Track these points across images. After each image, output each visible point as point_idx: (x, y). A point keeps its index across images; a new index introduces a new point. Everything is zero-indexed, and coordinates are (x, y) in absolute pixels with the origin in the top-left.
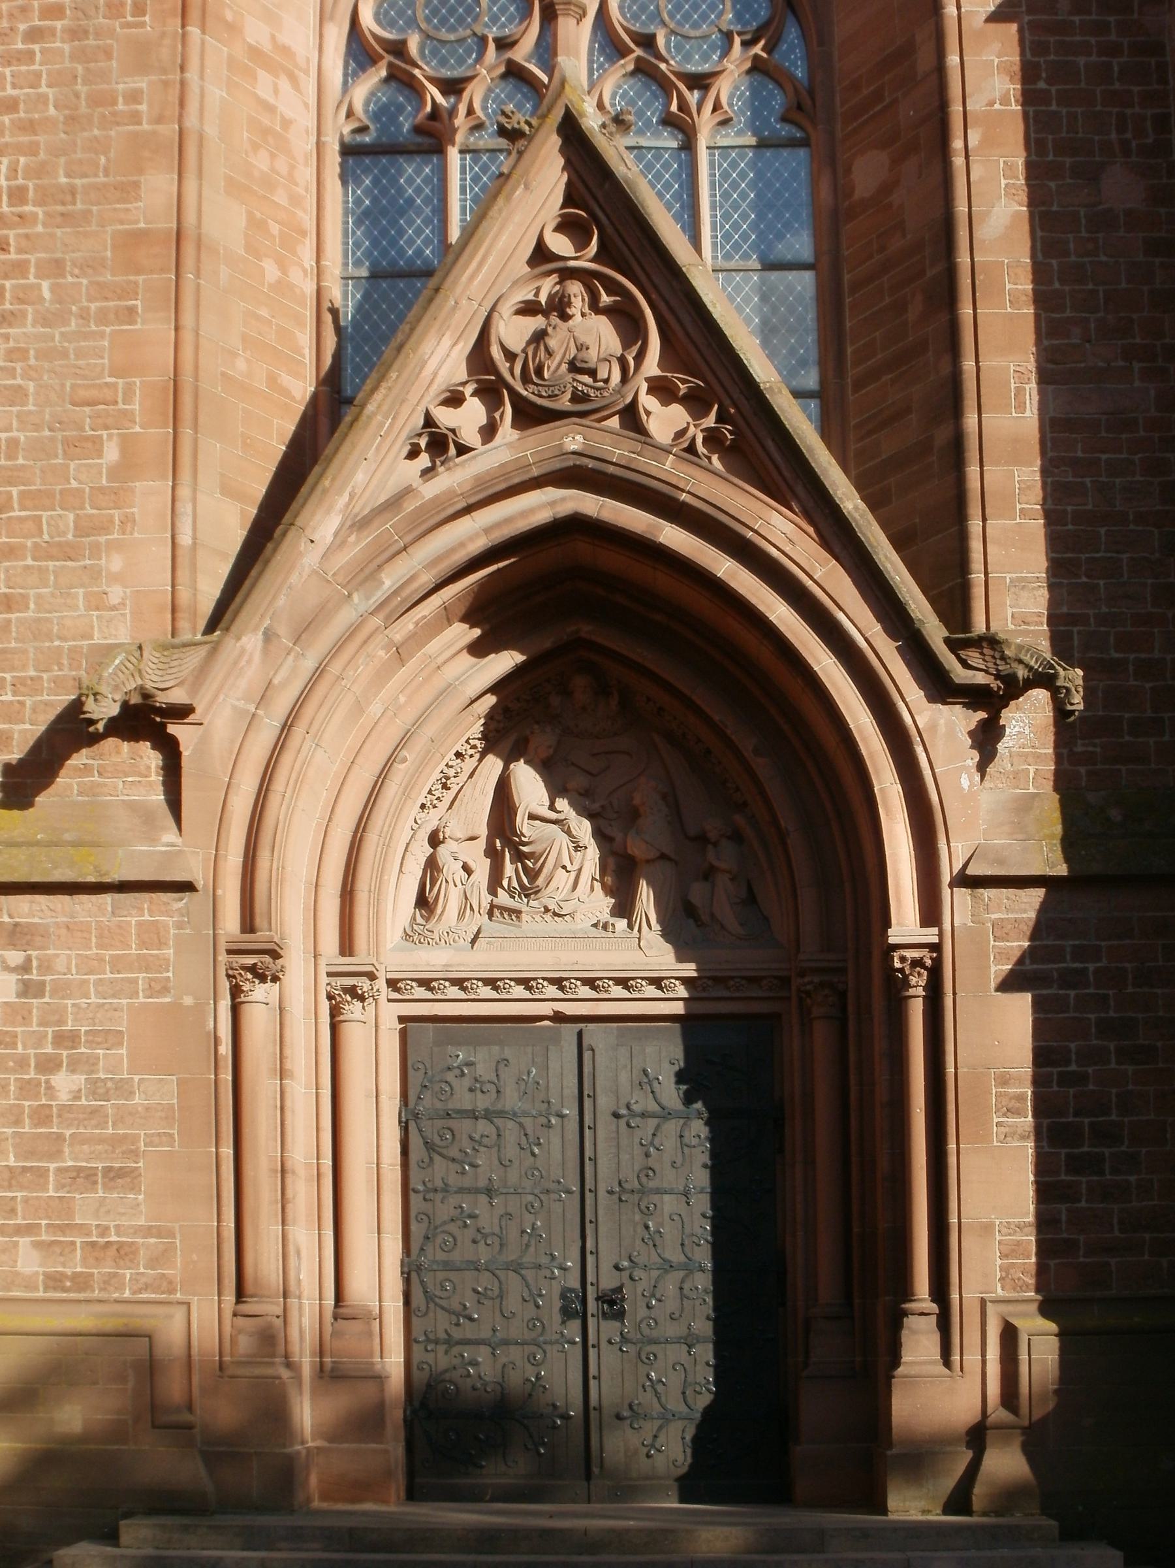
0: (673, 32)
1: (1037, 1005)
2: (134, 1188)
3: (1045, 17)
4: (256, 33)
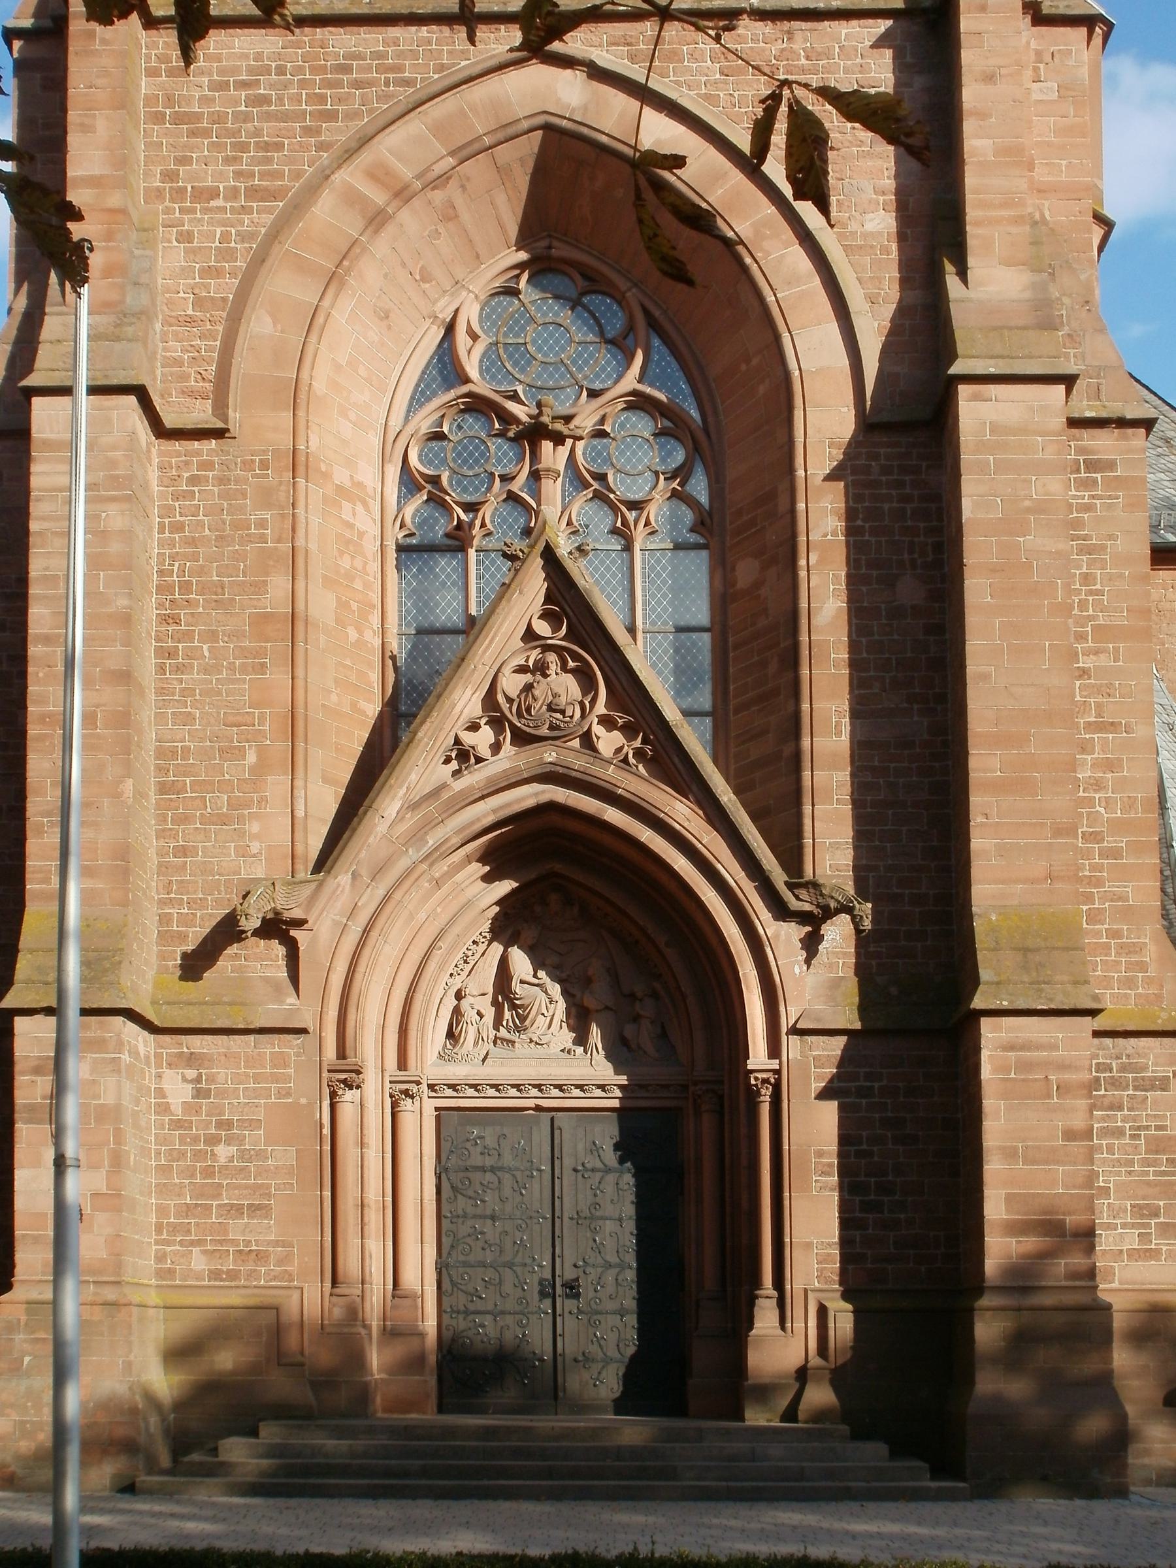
1: (842, 1109)
2: (268, 1216)
3: (862, 477)
4: (341, 476)
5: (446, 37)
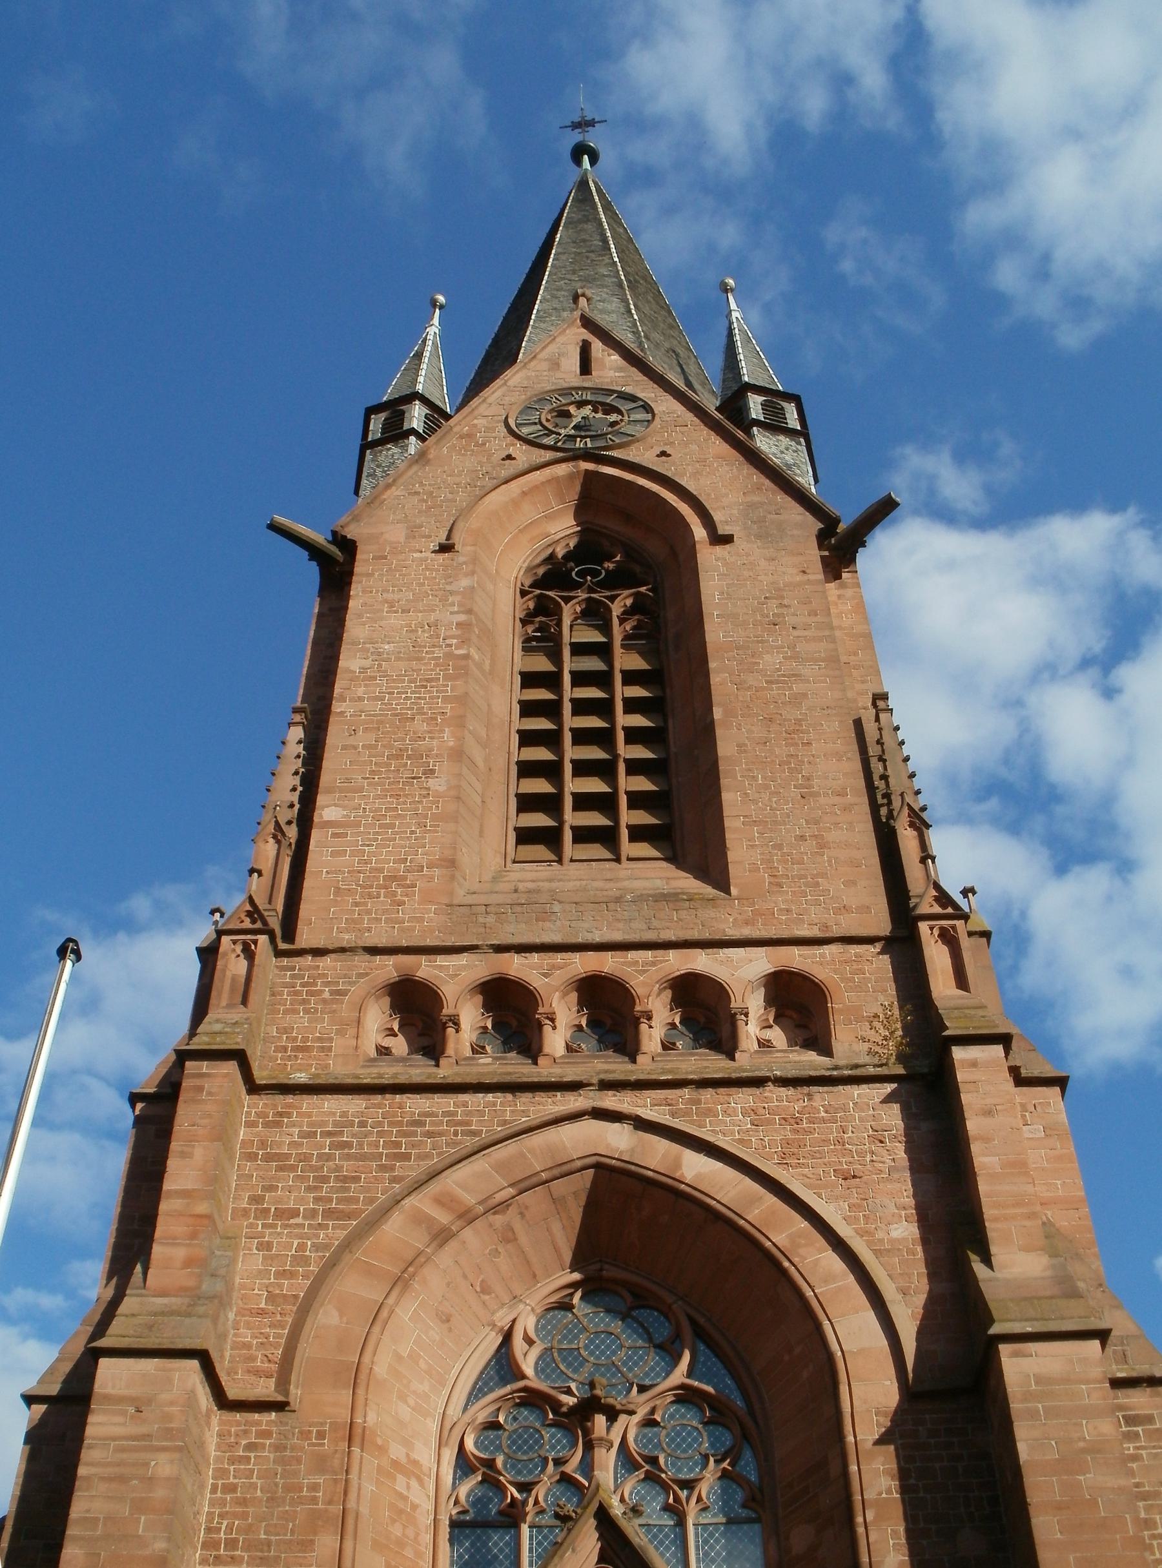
0: (669, 1455)
4: (397, 1451)
5: (510, 1101)
